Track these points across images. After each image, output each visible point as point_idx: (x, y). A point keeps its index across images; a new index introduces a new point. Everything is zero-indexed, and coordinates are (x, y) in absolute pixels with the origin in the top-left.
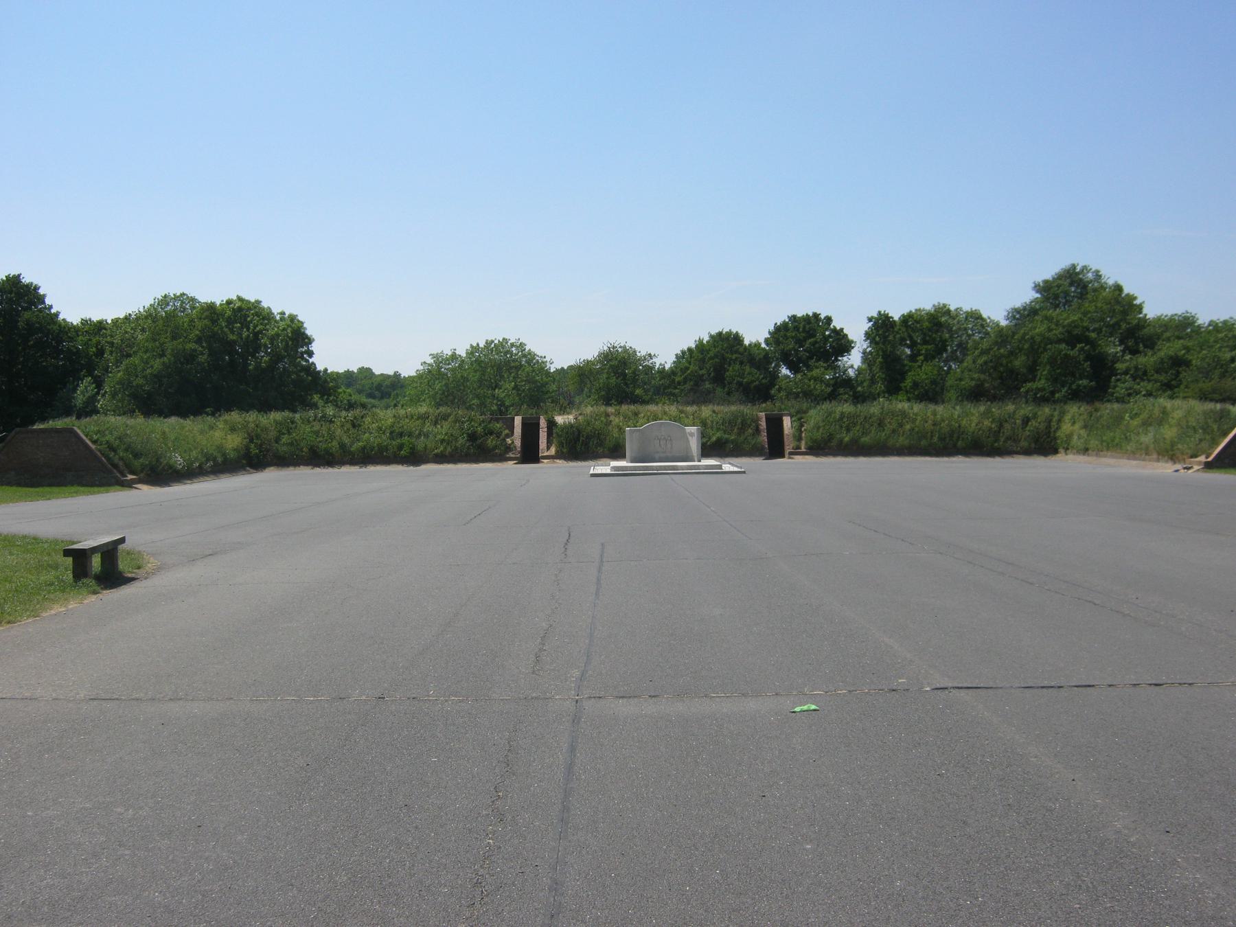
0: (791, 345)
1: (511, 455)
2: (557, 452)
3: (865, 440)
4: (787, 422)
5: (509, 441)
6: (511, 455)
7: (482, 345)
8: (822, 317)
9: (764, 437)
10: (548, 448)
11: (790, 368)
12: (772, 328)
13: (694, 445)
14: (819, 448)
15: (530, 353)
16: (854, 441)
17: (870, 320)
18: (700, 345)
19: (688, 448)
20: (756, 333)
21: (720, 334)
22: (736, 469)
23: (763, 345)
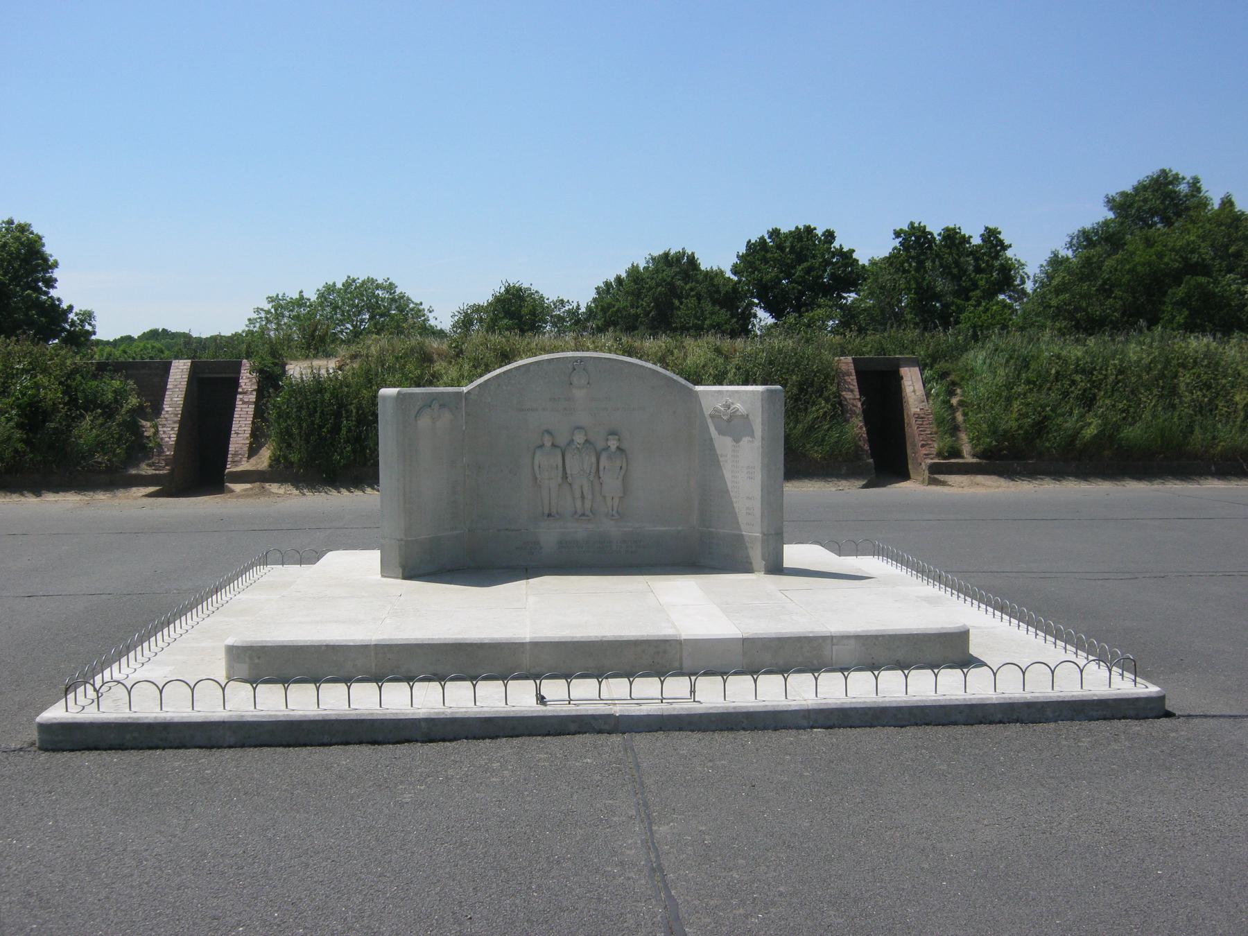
0: (771, 273)
1: (145, 470)
2: (275, 460)
3: (1132, 433)
4: (912, 382)
5: (147, 426)
6: (145, 470)
7: (339, 285)
8: (819, 232)
9: (857, 427)
10: (253, 451)
11: (769, 308)
12: (743, 250)
13: (745, 468)
14: (1010, 455)
15: (402, 297)
16: (1107, 437)
17: (897, 234)
18: (634, 272)
19: (711, 493)
20: (719, 255)
21: (666, 255)
22: (1125, 686)
23: (729, 274)
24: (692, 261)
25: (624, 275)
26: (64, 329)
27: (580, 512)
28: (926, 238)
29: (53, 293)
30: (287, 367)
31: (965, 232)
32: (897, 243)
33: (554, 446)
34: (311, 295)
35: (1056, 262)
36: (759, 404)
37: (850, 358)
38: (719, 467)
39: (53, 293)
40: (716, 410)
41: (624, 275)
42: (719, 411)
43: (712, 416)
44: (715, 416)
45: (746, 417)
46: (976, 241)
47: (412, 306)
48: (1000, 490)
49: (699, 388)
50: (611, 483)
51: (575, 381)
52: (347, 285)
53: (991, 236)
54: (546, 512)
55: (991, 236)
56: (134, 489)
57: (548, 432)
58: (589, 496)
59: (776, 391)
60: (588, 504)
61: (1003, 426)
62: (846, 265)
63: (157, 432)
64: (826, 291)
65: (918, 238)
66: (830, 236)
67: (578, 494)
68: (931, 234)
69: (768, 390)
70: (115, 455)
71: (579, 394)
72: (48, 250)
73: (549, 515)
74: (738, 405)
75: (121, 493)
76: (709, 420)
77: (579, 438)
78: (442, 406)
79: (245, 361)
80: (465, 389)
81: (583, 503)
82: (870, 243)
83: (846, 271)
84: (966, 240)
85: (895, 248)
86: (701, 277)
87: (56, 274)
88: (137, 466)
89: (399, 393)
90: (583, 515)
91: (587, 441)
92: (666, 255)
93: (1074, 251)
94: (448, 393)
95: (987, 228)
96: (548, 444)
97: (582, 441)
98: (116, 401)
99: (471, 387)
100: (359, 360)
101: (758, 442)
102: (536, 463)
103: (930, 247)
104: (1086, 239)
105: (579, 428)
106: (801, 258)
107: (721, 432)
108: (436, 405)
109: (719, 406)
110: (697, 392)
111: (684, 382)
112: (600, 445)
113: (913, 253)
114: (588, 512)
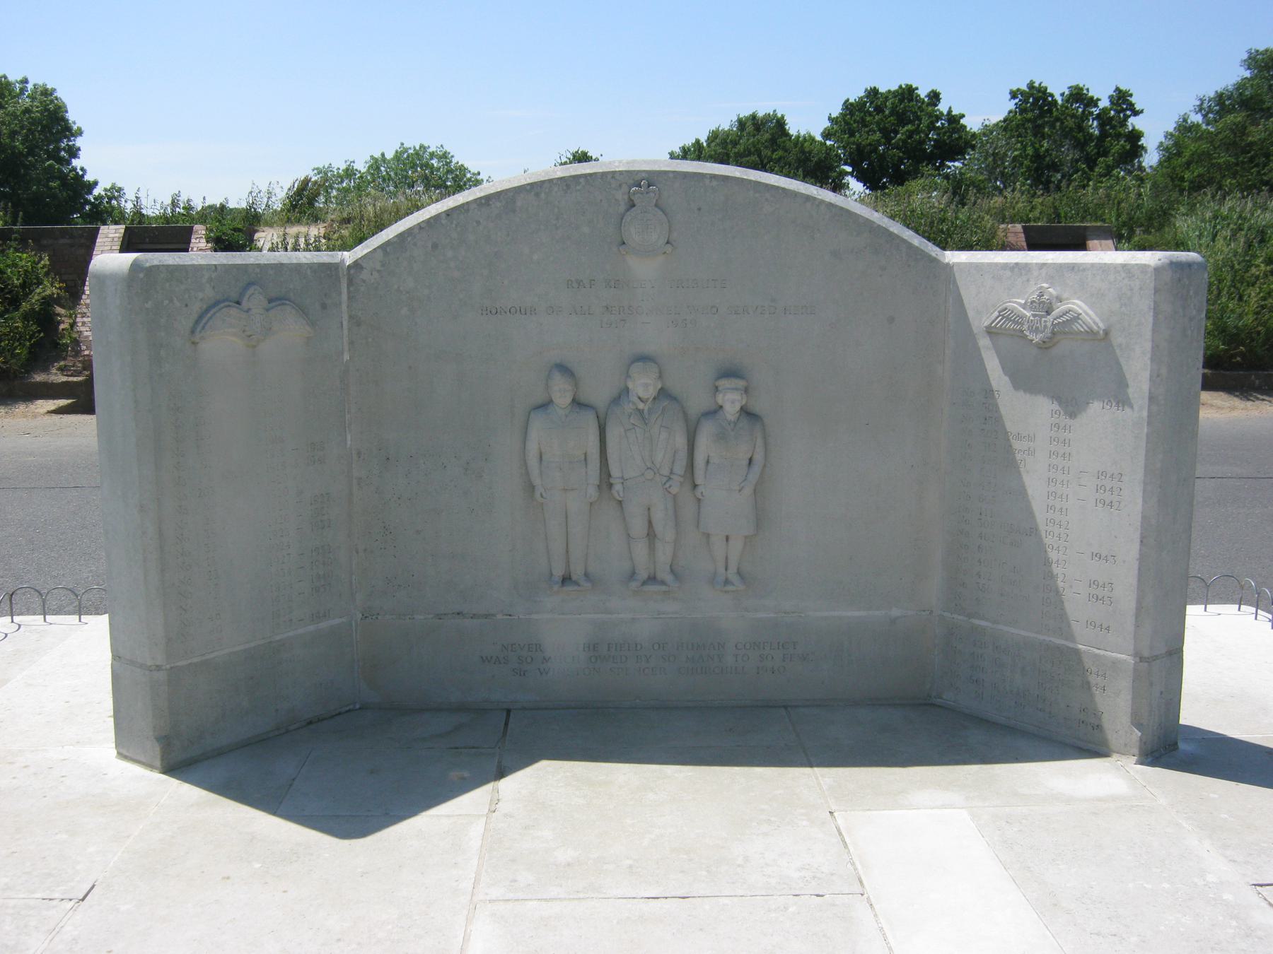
0: (862, 138)
12: (836, 111)
17: (1013, 95)
24: (781, 123)
25: (703, 140)
26: (88, 202)
27: (643, 574)
28: (1045, 100)
29: (76, 163)
30: (257, 236)
31: (1093, 93)
32: (1011, 105)
33: (578, 404)
34: (361, 166)
35: (1185, 128)
36: (1144, 303)
37: (1019, 227)
38: (1010, 464)
39: (75, 162)
40: (1006, 315)
41: (703, 140)
42: (1019, 319)
43: (990, 331)
44: (1006, 332)
45: (1101, 339)
46: (1104, 103)
47: (468, 176)
48: (1235, 414)
49: (955, 257)
50: (724, 499)
51: (633, 233)
52: (398, 156)
53: (1122, 100)
54: (559, 572)
55: (1122, 100)
56: (40, 402)
57: (564, 369)
58: (665, 531)
59: (1189, 265)
60: (664, 553)
61: (1231, 321)
62: (954, 130)
63: (73, 325)
64: (930, 159)
65: (1036, 100)
66: (935, 97)
67: (638, 527)
68: (1052, 95)
69: (1176, 266)
70: (13, 356)
71: (644, 269)
72: (71, 116)
73: (566, 580)
74: (1077, 305)
75: (21, 408)
76: (984, 342)
77: (643, 385)
78: (275, 301)
79: (197, 227)
80: (348, 257)
81: (652, 548)
82: (981, 106)
83: (954, 139)
84: (1093, 102)
85: (1010, 112)
86: (788, 144)
87: (79, 142)
88: (46, 370)
89: (135, 266)
90: (652, 579)
91: (663, 393)
92: (754, 117)
93: (1205, 116)
94: (298, 268)
95: (1117, 89)
96: (562, 398)
97: (651, 392)
98: (23, 286)
99: (361, 251)
100: (350, 226)
101: (1138, 412)
102: (533, 448)
103: (1050, 111)
104: (1222, 104)
105: (643, 358)
106: (902, 119)
107: (1023, 380)
108: (255, 300)
109: (1017, 304)
110: (949, 268)
111: (916, 240)
112: (697, 402)
113: (1030, 115)
114: (664, 574)
